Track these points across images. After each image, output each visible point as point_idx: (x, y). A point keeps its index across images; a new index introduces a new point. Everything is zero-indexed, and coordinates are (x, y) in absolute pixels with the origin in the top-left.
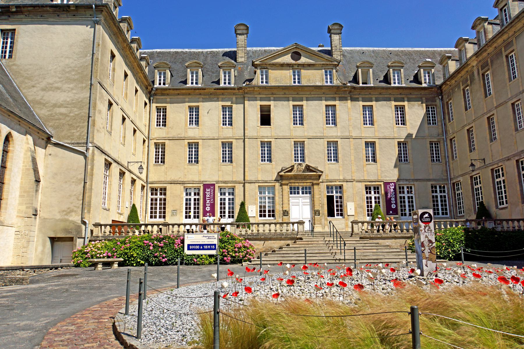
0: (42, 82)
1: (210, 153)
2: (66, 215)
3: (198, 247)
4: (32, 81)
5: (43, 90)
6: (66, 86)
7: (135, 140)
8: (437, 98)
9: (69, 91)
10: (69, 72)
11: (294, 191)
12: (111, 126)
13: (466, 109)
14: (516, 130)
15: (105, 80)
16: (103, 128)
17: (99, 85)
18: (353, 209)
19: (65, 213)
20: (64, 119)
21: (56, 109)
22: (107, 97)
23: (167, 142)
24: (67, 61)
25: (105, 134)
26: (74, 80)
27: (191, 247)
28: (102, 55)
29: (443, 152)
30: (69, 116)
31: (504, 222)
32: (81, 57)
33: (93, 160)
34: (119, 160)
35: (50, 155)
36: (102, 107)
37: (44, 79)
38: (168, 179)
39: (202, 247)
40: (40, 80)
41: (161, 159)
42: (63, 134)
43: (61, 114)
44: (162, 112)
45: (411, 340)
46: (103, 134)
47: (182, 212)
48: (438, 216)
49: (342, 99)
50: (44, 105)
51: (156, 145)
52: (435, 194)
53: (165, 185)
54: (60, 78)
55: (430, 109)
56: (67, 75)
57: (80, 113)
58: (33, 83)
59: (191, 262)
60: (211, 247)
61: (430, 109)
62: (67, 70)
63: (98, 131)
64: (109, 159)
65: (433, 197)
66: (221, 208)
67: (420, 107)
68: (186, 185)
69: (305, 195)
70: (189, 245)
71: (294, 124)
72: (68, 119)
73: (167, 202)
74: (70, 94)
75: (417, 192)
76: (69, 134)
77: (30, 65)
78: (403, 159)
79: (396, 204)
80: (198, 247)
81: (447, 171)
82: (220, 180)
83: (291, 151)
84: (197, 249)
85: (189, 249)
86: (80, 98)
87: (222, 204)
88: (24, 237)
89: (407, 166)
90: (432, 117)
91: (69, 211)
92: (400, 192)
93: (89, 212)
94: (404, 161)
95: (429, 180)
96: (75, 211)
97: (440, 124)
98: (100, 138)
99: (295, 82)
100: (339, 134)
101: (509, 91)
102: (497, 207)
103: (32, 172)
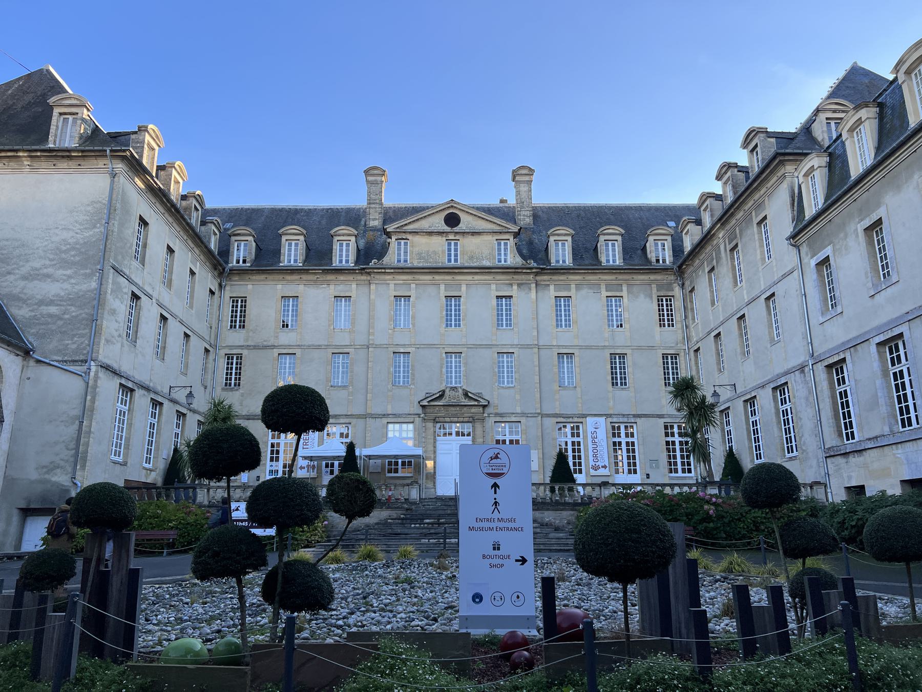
0: (23, 266)
4: (8, 265)
5: (25, 278)
6: (61, 272)
9: (64, 281)
10: (65, 252)
12: (137, 332)
13: (713, 304)
15: (126, 262)
16: (120, 336)
17: (112, 270)
19: (45, 470)
20: (54, 324)
21: (42, 307)
22: (127, 288)
23: (245, 352)
24: (66, 235)
25: (122, 346)
26: (74, 264)
28: (122, 225)
30: (61, 319)
32: (86, 229)
33: (95, 386)
35: (29, 379)
36: (119, 305)
37: (27, 261)
40: (21, 263)
42: (51, 347)
43: (50, 316)
44: (240, 307)
46: (119, 345)
48: (676, 475)
50: (24, 301)
51: (229, 357)
52: (670, 439)
54: (51, 260)
55: (664, 303)
56: (63, 256)
57: (81, 314)
58: (9, 268)
61: (664, 303)
62: (64, 248)
63: (107, 341)
64: (130, 385)
65: (667, 443)
67: (648, 300)
71: (447, 325)
72: (60, 323)
74: (66, 286)
75: (640, 435)
76: (61, 347)
77: (7, 240)
78: (619, 381)
83: (442, 367)
86: (80, 290)
89: (624, 392)
90: (668, 315)
91: (52, 468)
93: (83, 467)
94: (621, 384)
95: (661, 416)
96: (62, 467)
97: (679, 326)
98: (108, 353)
99: (450, 260)
101: (762, 279)
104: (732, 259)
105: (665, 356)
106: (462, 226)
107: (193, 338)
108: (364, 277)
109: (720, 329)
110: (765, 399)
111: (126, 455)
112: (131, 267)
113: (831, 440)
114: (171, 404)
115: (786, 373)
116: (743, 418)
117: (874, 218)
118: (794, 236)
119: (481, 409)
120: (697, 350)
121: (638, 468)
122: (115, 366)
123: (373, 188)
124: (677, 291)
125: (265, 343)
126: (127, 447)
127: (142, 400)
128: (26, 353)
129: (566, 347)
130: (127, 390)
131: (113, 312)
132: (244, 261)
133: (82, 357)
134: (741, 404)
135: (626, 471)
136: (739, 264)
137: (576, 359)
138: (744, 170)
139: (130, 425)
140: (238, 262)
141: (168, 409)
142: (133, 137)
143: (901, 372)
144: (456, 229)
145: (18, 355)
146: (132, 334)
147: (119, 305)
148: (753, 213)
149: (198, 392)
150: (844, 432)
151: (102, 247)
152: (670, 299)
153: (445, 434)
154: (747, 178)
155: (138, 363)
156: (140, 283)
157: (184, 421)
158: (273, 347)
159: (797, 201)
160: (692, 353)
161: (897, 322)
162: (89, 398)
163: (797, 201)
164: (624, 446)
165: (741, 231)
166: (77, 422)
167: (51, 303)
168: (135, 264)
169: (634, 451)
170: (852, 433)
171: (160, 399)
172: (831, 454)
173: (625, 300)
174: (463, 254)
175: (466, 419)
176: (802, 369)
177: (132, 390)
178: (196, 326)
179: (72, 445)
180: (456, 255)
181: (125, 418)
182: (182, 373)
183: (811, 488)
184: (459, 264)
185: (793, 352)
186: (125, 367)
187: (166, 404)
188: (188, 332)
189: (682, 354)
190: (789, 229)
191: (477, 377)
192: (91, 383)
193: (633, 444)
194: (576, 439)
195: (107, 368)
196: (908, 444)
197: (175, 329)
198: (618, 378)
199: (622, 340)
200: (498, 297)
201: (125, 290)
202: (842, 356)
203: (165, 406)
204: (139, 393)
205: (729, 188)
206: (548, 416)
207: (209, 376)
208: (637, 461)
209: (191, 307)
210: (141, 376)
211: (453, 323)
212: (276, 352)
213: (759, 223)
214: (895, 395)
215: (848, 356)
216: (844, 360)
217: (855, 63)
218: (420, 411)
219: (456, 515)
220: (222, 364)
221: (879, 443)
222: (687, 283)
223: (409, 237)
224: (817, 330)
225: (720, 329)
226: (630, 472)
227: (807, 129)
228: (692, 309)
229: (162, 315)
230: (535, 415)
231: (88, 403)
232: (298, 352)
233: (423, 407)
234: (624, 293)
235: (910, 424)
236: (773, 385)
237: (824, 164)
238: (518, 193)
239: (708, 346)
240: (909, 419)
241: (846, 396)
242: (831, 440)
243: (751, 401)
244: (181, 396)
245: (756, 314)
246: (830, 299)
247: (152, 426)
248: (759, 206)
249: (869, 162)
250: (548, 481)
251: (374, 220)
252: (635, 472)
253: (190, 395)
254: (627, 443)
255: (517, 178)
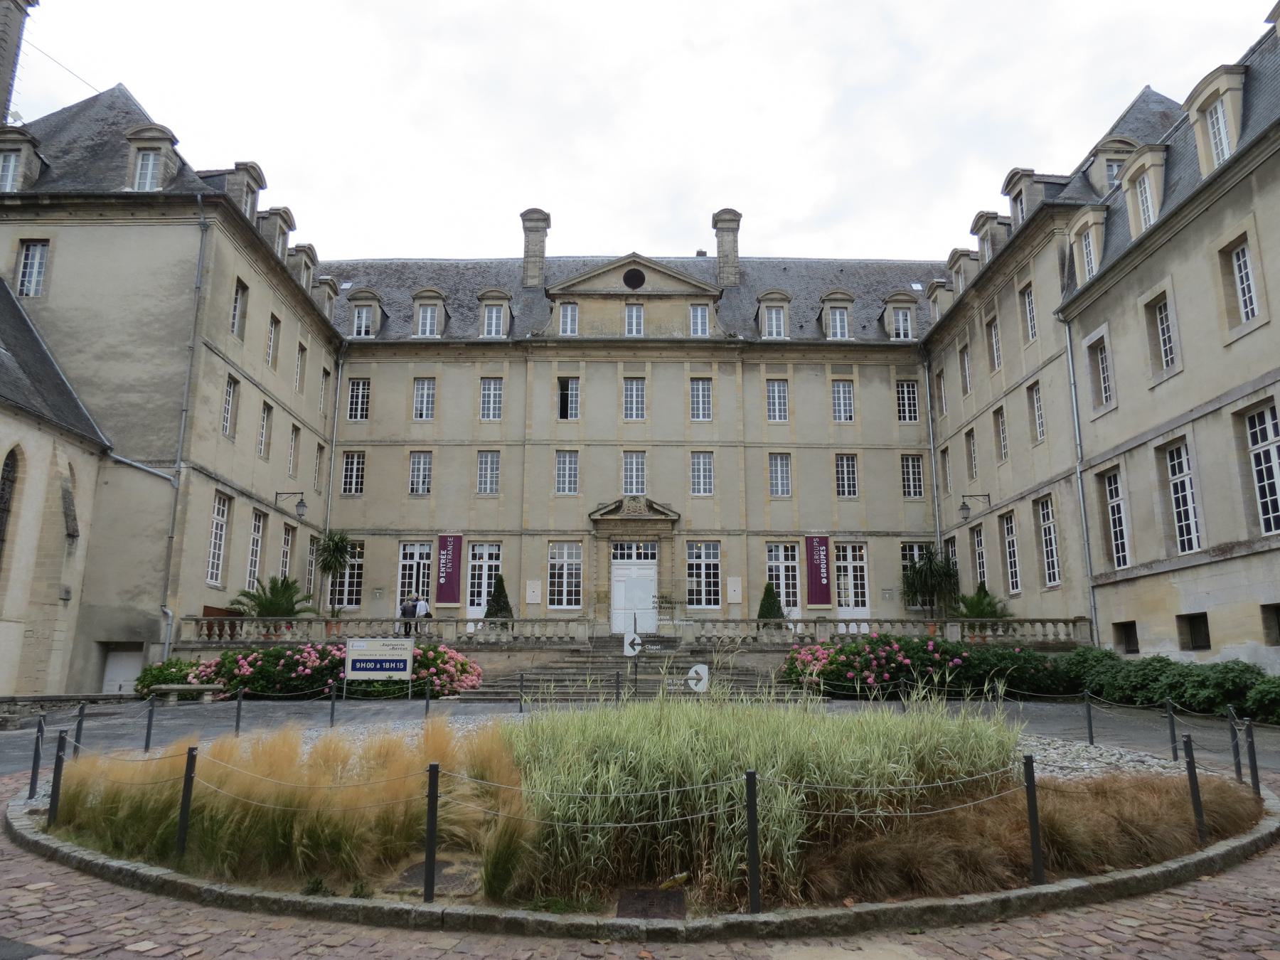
1: (454, 474)
2: (132, 599)
3: (371, 665)
5: (99, 357)
7: (296, 448)
8: (919, 366)
11: (621, 551)
13: (965, 391)
14: (1035, 439)
16: (214, 430)
17: (204, 348)
18: (739, 591)
22: (223, 370)
23: (368, 450)
25: (218, 443)
27: (358, 665)
29: (927, 477)
31: (1049, 626)
33: (187, 493)
34: (254, 491)
36: (212, 391)
38: (369, 526)
39: (379, 665)
41: (355, 481)
43: (131, 405)
45: (440, 780)
47: (395, 592)
49: (726, 365)
51: (349, 455)
53: (361, 538)
54: (131, 335)
59: (365, 692)
60: (399, 665)
64: (228, 491)
66: (473, 585)
68: (403, 538)
69: (643, 561)
70: (354, 662)
73: (364, 571)
79: (828, 578)
80: (371, 665)
81: (934, 516)
82: (473, 528)
84: (370, 670)
85: (354, 668)
87: (476, 576)
88: (36, 641)
91: (137, 593)
92: (838, 558)
93: (175, 593)
95: (897, 535)
97: (924, 418)
98: (204, 451)
99: (630, 331)
100: (716, 438)
102: (1007, 590)
103: (61, 518)
104: (989, 335)
105: (840, 457)
106: (647, 288)
107: (303, 432)
108: (519, 353)
109: (973, 425)
110: (1024, 514)
111: (225, 578)
112: (227, 342)
113: (1100, 567)
114: (278, 515)
115: (1051, 482)
116: (998, 540)
117: (1156, 290)
118: (1062, 310)
119: (670, 525)
120: (944, 452)
121: (867, 599)
122: (211, 468)
123: (532, 236)
124: (922, 376)
125: (394, 438)
126: (226, 569)
127: (243, 509)
128: (103, 452)
129: (780, 445)
130: (225, 499)
131: (206, 400)
132: (367, 333)
133: (170, 457)
134: (996, 520)
135: (852, 602)
136: (997, 342)
137: (793, 460)
138: (1005, 223)
139: (228, 541)
140: (359, 333)
141: (275, 523)
142: (227, 177)
143: (1183, 483)
144: (639, 291)
145: (92, 454)
146: (1050, 572)
147: (212, 391)
148: (1016, 279)
149: (311, 499)
150: (1115, 556)
151: (192, 318)
152: (912, 384)
153: (622, 557)
154: (1009, 232)
155: (240, 465)
156: (238, 362)
157: (294, 536)
158: (403, 444)
159: (1067, 266)
160: (939, 454)
161: (1181, 422)
162: (179, 507)
163: (1067, 266)
164: (851, 573)
165: (1000, 301)
166: (166, 538)
167: (131, 389)
168: (233, 338)
169: (862, 578)
170: (1124, 557)
171: (264, 509)
172: (1099, 584)
173: (856, 384)
174: (647, 322)
175: (650, 538)
176: (1067, 477)
177: (231, 499)
178: (306, 415)
179: (161, 566)
180: (638, 324)
181: (223, 531)
182: (290, 476)
183: (1074, 625)
184: (642, 336)
185: (1056, 456)
186: (222, 470)
187: (273, 516)
188: (298, 424)
189: (926, 455)
190: (1057, 300)
191: (667, 484)
192: (181, 488)
193: (862, 569)
194: (790, 563)
195: (200, 470)
196: (1188, 572)
197: (281, 422)
198: (846, 486)
199: (851, 438)
200: (693, 379)
201: (221, 373)
202: (1115, 462)
203: (271, 517)
204: (239, 502)
205: (988, 246)
206: (757, 534)
207: (324, 479)
208: (867, 590)
209: (301, 391)
210: (242, 481)
211: (634, 412)
212: (407, 449)
213: (1022, 293)
214: (1175, 511)
215: (1121, 461)
216: (1117, 467)
217: (1148, 87)
218: (590, 526)
219: (526, 229)
220: (341, 464)
221: (1154, 572)
222: (934, 364)
223: (579, 301)
224: (1087, 429)
225: (973, 425)
226: (857, 604)
227: (1083, 173)
228: (940, 398)
229: (265, 403)
230: (738, 533)
231: (178, 514)
232: (435, 450)
233: (595, 522)
234: (855, 376)
235: (1191, 548)
236: (1034, 497)
237: (1101, 221)
238: (720, 245)
239: (958, 447)
240: (1190, 541)
241: (1119, 512)
242: (1100, 567)
243: (1007, 518)
244: (289, 504)
245: (1016, 407)
246: (1102, 391)
247: (255, 542)
248: (1023, 270)
249: (1153, 220)
250: (755, 616)
251: (534, 277)
252: (864, 604)
253: (301, 504)
254: (855, 568)
255: (719, 225)
